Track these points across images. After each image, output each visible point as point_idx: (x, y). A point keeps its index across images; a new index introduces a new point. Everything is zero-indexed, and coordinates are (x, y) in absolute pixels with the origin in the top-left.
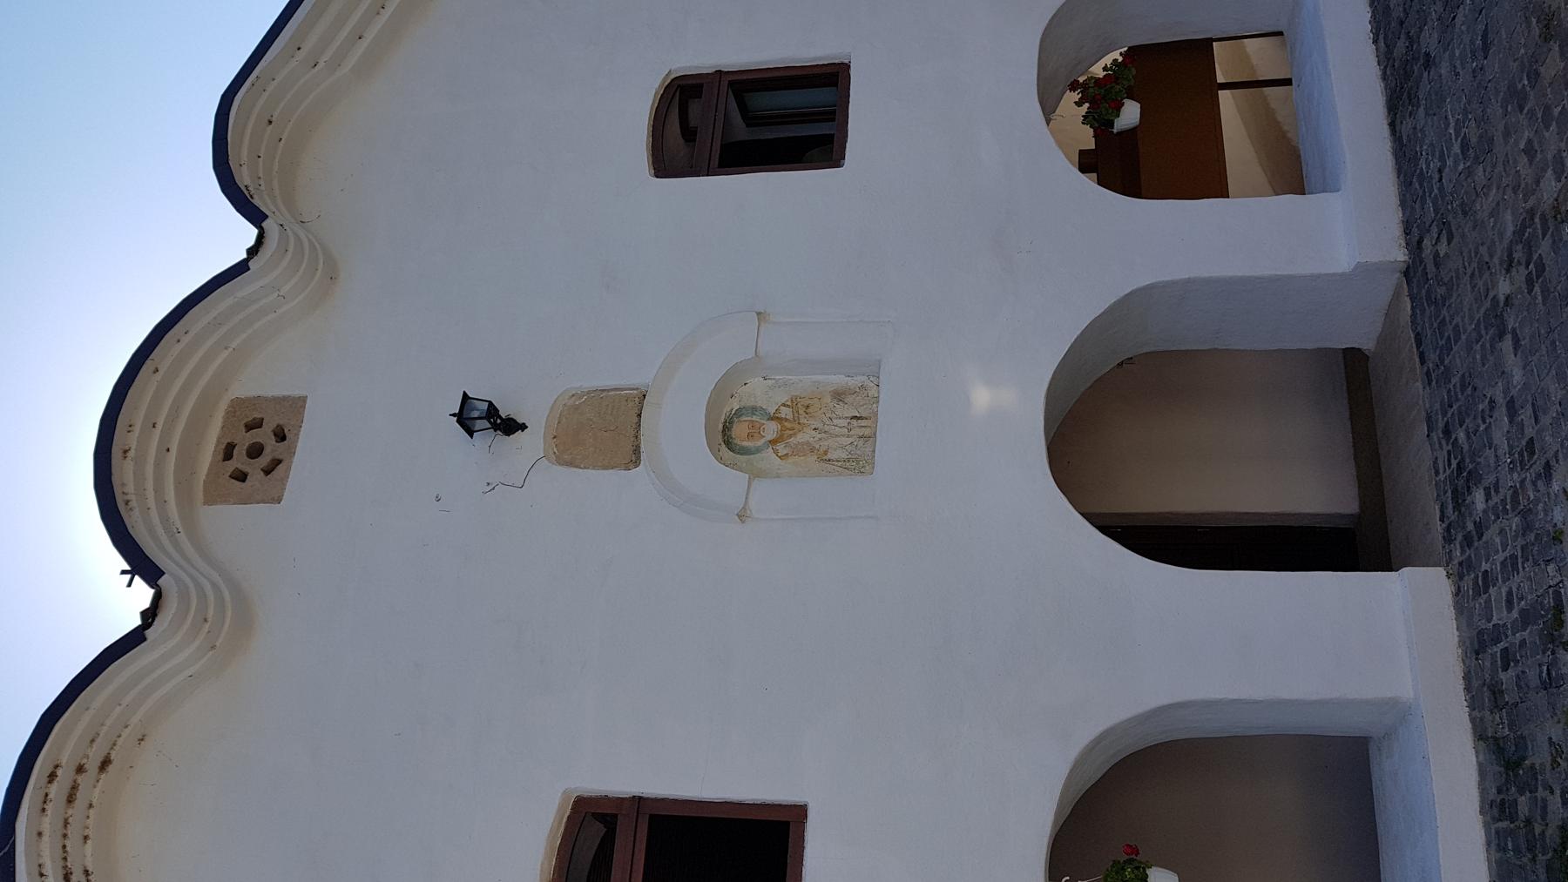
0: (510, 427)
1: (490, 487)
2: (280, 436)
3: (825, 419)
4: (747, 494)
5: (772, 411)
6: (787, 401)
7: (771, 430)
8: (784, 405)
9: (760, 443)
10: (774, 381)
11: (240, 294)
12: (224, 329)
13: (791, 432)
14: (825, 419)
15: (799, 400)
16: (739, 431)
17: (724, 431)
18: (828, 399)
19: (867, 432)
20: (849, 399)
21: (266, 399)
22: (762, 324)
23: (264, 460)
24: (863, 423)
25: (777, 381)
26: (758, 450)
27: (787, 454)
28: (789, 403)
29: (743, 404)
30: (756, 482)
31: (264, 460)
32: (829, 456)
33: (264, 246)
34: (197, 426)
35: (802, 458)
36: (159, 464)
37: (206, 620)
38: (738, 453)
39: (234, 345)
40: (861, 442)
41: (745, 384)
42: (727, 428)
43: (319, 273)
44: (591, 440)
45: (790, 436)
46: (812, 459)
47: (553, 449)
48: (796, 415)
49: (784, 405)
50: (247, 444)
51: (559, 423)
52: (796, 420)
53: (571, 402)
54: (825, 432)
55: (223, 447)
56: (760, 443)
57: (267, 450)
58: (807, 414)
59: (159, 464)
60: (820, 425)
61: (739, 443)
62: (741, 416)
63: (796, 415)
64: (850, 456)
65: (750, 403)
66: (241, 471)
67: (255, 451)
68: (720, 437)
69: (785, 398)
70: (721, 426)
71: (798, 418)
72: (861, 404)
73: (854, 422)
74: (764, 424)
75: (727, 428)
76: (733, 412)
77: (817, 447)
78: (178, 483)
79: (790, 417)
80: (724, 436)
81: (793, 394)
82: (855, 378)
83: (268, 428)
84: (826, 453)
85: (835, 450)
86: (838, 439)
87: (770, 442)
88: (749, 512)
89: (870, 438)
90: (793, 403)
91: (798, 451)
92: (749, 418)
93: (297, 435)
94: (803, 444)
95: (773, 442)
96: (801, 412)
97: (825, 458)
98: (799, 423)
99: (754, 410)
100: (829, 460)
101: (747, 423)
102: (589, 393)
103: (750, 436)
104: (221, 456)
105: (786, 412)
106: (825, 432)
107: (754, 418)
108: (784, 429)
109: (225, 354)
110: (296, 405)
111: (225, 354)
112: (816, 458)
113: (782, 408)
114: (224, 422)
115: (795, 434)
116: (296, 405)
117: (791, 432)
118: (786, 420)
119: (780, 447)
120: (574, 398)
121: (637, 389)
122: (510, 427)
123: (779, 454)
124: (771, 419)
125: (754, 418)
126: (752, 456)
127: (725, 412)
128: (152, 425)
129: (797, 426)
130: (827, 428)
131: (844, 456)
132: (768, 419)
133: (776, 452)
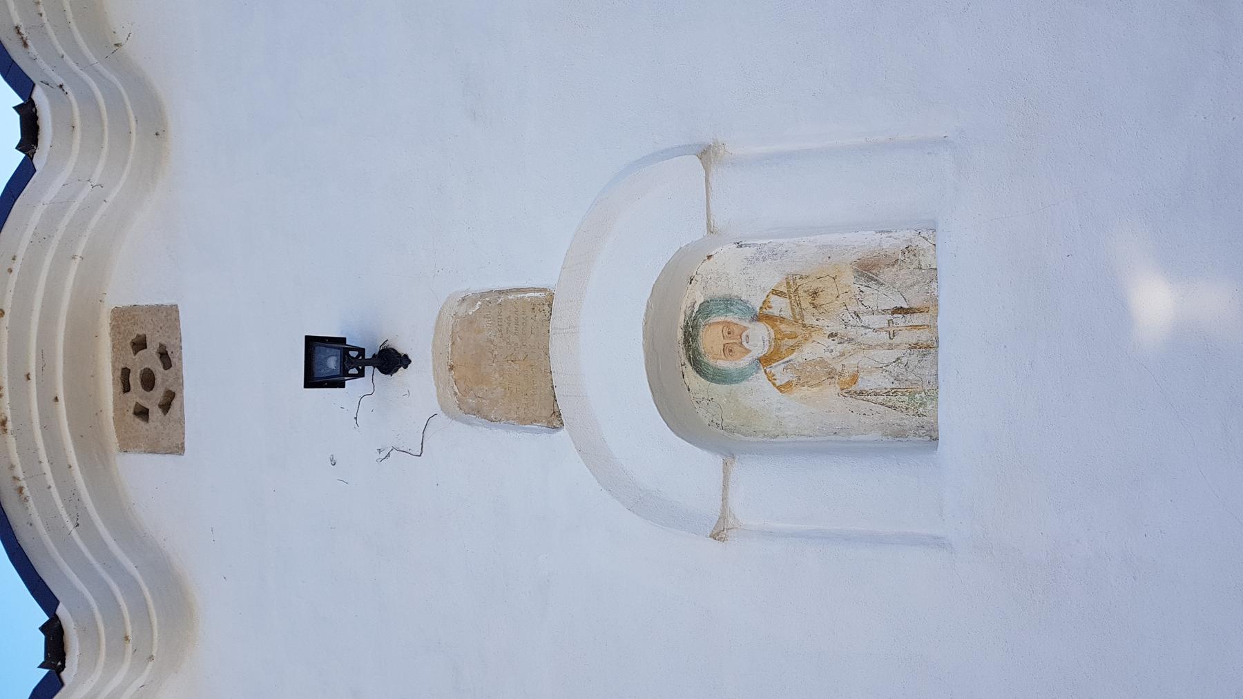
0: (391, 361)
1: (383, 454)
2: (165, 358)
3: (848, 317)
4: (725, 487)
5: (757, 304)
6: (780, 284)
7: (759, 338)
8: (776, 292)
9: (744, 362)
10: (753, 249)
11: (49, 196)
12: (55, 243)
13: (791, 342)
14: (848, 317)
15: (799, 282)
16: (710, 340)
17: (686, 341)
18: (848, 278)
19: (923, 336)
20: (887, 275)
21: (141, 308)
22: (713, 170)
23: (135, 380)
24: (916, 319)
25: (759, 248)
26: (742, 376)
27: (789, 383)
28: (783, 289)
29: (709, 293)
30: (737, 469)
31: (135, 380)
32: (861, 385)
33: (40, 128)
34: (79, 361)
35: (815, 389)
36: (49, 426)
37: (126, 638)
38: (713, 380)
39: (79, 253)
40: (914, 358)
41: (709, 257)
42: (690, 336)
43: (134, 135)
44: (497, 375)
45: (792, 349)
46: (832, 390)
47: (453, 387)
48: (797, 310)
49: (776, 292)
50: (139, 371)
51: (453, 344)
52: (798, 319)
53: (462, 310)
54: (850, 340)
55: (120, 373)
56: (744, 362)
57: (158, 381)
58: (815, 307)
59: (49, 426)
60: (837, 327)
61: (712, 362)
62: (708, 315)
63: (797, 310)
64: (896, 385)
65: (719, 290)
66: (140, 405)
67: (148, 381)
68: (682, 351)
69: (773, 279)
70: (680, 335)
71: (802, 316)
72: (909, 282)
73: (899, 319)
74: (745, 328)
75: (690, 336)
76: (696, 309)
77: (839, 369)
78: (78, 438)
79: (787, 313)
80: (687, 351)
81: (788, 270)
82: (895, 235)
83: (152, 349)
84: (854, 379)
85: (870, 372)
86: (872, 352)
87: (759, 360)
88: (730, 520)
89: (927, 349)
90: (790, 289)
91: (808, 376)
92: (722, 319)
93: (180, 359)
94: (814, 363)
95: (765, 361)
96: (806, 304)
97: (853, 388)
98: (804, 326)
99: (728, 303)
100: (861, 393)
101: (721, 327)
102: (482, 295)
103: (728, 351)
104: (120, 387)
105: (780, 306)
106: (850, 340)
107: (730, 318)
108: (779, 337)
109: (74, 267)
110: (170, 315)
111: (74, 267)
112: (838, 390)
113: (773, 298)
114: (113, 340)
115: (798, 345)
116: (170, 315)
117: (791, 342)
118: (782, 319)
119: (777, 369)
120: (465, 305)
121: (544, 290)
122: (391, 361)
123: (778, 383)
124: (758, 318)
125: (730, 318)
126: (734, 386)
127: (683, 308)
128: (25, 378)
129: (800, 331)
130: (852, 332)
131: (886, 383)
132: (753, 320)
133: (771, 378)
